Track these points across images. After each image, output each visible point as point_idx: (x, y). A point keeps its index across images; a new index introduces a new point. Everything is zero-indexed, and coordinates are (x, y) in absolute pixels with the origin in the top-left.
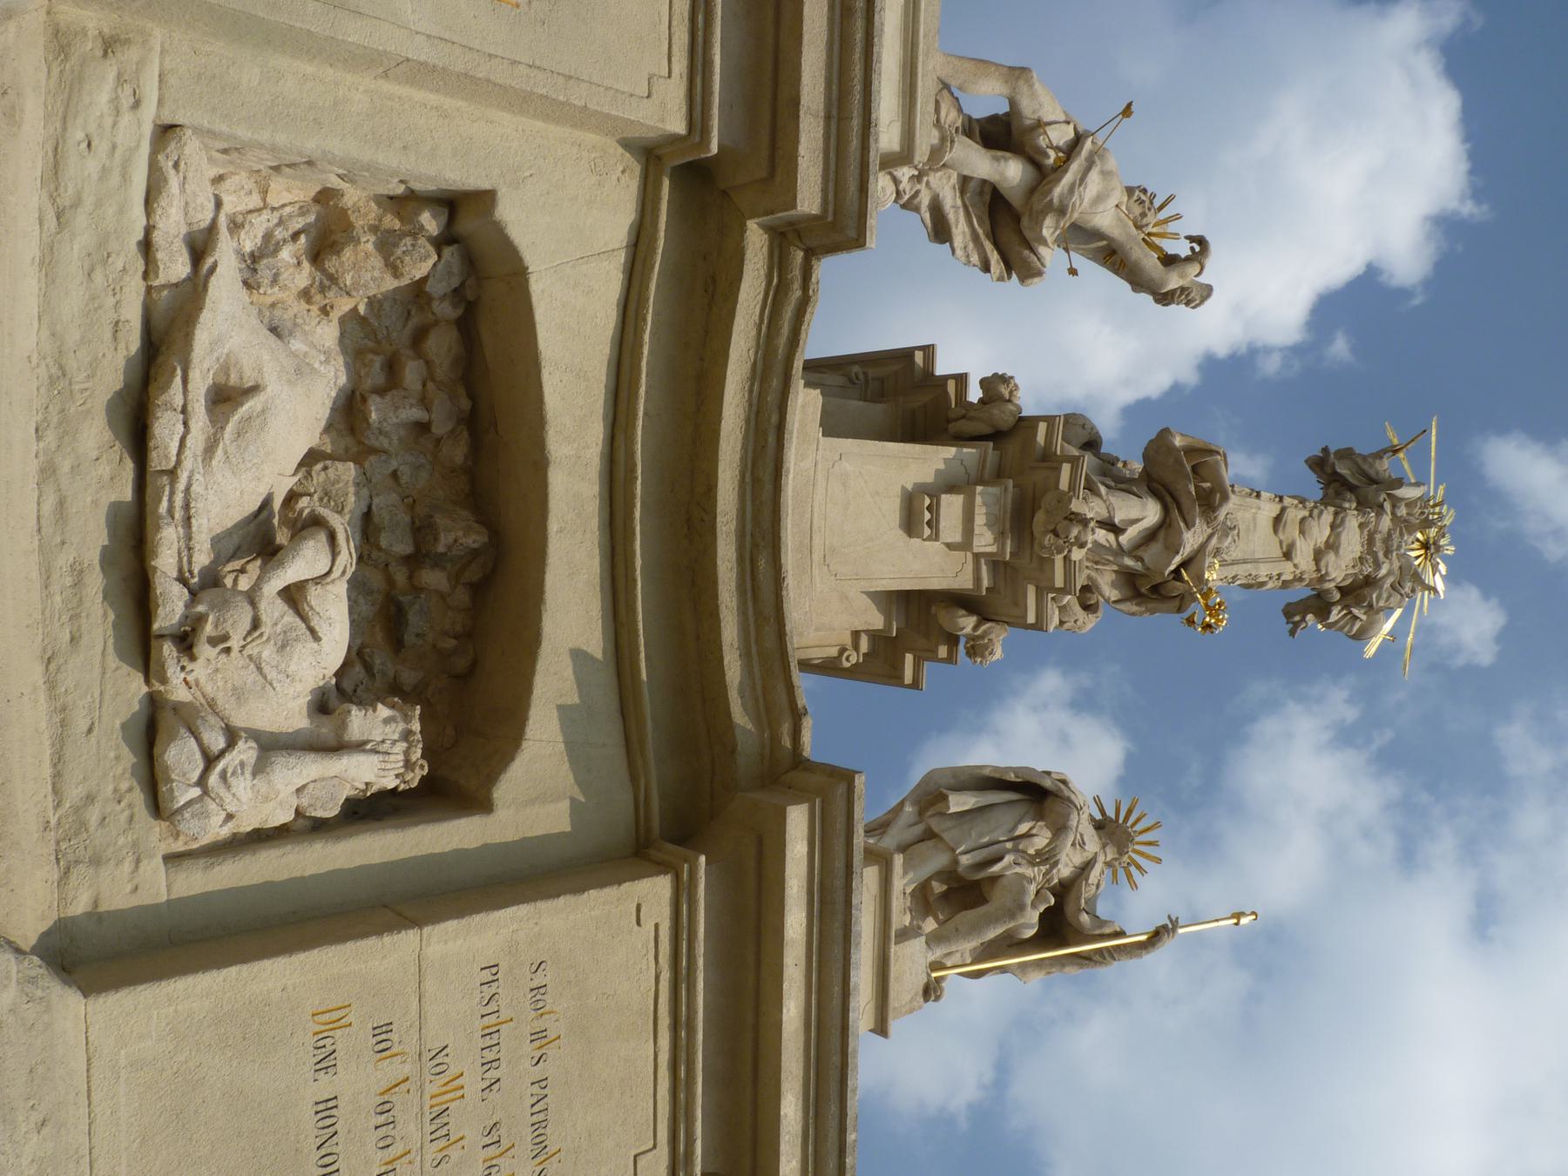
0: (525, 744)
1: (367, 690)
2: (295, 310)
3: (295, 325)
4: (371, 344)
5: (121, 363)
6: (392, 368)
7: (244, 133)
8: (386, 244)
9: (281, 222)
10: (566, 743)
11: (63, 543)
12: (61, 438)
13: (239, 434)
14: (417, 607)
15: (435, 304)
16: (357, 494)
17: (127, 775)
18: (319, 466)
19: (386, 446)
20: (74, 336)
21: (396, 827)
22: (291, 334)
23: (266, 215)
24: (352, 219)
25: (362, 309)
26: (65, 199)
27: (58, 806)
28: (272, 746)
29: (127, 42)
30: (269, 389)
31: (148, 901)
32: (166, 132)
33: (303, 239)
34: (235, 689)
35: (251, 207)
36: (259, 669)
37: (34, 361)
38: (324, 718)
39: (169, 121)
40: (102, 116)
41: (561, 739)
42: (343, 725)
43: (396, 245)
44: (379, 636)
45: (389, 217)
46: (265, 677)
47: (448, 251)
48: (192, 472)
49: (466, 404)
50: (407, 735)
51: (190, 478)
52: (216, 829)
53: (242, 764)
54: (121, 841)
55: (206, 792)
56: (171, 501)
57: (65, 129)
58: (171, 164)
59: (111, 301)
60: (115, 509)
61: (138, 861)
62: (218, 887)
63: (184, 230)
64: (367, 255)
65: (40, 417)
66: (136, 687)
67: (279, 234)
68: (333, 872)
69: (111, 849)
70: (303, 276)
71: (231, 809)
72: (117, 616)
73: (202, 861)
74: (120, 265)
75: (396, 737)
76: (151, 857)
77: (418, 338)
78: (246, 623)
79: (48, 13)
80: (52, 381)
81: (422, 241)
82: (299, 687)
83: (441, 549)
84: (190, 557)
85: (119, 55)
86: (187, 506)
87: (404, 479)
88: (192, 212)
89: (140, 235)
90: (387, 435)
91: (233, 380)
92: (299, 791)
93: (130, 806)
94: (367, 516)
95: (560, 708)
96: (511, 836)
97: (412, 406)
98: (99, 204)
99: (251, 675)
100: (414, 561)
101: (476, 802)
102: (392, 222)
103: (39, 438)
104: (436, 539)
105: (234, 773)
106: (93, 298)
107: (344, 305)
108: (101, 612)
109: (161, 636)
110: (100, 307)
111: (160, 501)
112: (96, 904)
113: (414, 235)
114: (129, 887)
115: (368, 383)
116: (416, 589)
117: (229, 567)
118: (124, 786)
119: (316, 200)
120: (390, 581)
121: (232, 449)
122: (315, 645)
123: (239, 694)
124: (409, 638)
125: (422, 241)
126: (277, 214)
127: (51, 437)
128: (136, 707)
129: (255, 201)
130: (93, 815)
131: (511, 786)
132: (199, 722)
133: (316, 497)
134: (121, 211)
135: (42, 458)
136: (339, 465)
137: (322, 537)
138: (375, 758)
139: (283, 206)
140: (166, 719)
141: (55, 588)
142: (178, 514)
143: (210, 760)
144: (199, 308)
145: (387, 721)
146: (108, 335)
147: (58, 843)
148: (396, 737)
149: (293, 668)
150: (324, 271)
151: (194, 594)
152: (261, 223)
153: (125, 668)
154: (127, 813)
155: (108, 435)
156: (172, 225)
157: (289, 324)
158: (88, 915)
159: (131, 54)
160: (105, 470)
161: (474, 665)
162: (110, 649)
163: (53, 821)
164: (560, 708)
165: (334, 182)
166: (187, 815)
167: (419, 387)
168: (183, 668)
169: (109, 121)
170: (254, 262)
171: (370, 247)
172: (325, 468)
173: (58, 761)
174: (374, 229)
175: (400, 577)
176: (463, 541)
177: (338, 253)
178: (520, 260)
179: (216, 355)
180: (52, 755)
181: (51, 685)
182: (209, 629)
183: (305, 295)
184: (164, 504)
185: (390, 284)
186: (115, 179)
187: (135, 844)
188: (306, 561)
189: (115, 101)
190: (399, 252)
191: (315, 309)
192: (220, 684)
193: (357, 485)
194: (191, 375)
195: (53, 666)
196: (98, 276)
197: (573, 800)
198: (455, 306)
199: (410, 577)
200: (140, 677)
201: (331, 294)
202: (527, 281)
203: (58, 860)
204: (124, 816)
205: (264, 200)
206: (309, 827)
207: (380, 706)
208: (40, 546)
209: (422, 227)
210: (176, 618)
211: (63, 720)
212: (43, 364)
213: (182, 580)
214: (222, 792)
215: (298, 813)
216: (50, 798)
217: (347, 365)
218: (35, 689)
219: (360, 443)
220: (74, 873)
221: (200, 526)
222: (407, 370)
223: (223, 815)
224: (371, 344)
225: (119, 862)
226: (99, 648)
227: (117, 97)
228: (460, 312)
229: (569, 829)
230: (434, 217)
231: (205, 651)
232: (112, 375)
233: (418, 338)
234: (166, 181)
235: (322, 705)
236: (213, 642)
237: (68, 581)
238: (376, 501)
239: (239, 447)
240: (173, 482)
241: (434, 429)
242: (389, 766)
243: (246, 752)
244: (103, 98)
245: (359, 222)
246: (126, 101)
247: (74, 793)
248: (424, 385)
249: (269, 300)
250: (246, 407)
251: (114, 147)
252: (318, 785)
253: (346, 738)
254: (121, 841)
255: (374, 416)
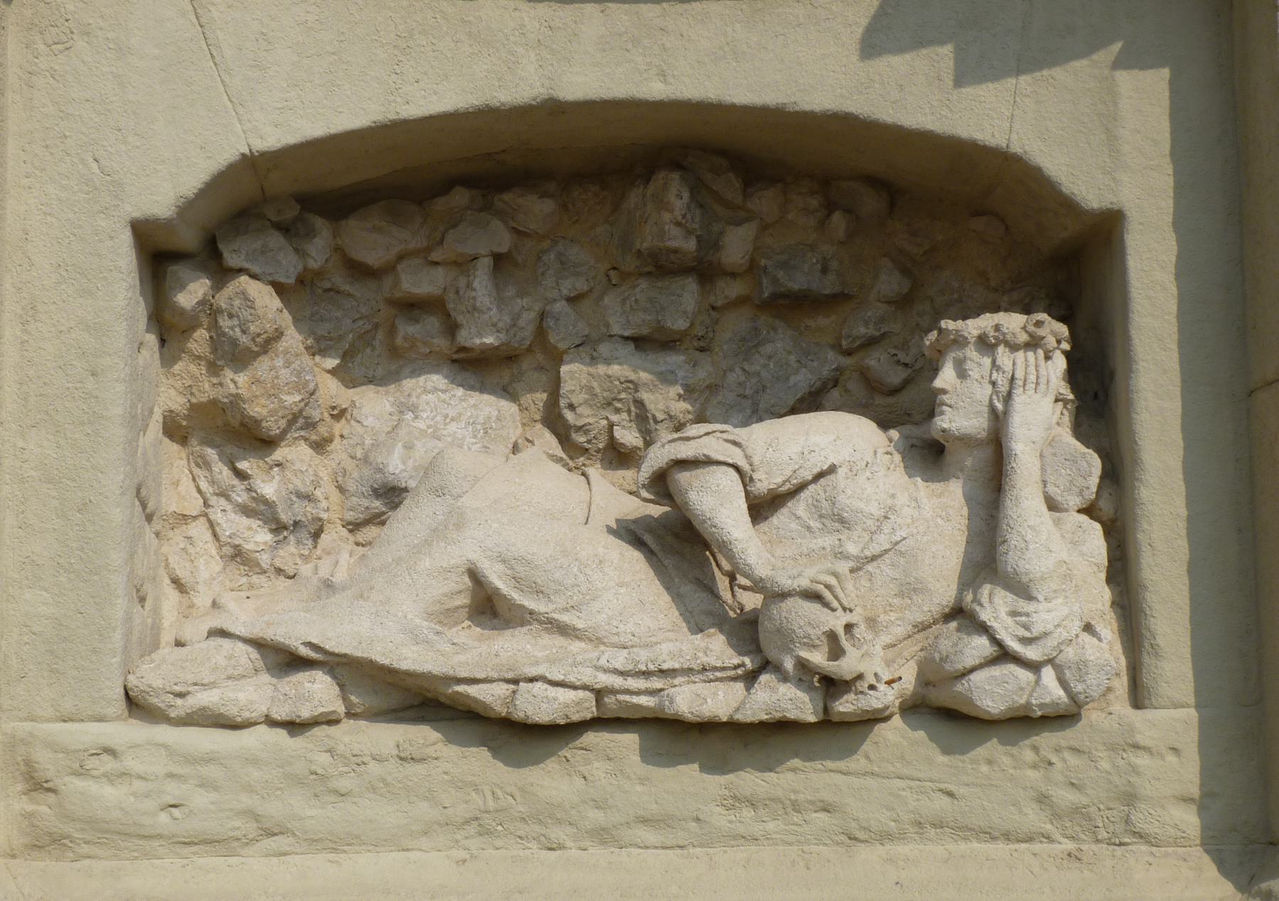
0: (1016, 148)
1: (904, 346)
2: (344, 456)
3: (366, 460)
4: (380, 335)
5: (453, 751)
6: (412, 307)
7: (118, 582)
8: (232, 354)
9: (224, 494)
10: (1019, 72)
11: (698, 820)
12: (559, 822)
13: (539, 592)
14: (780, 274)
15: (313, 264)
16: (608, 362)
17: (1015, 750)
18: (569, 416)
19: (532, 315)
20: (423, 810)
21: (1129, 370)
22: (380, 470)
23: (217, 516)
24: (203, 398)
25: (332, 363)
26: (250, 828)
27: (1049, 839)
28: (987, 558)
29: (28, 763)
30: (473, 556)
31: (1194, 734)
32: (135, 705)
33: (243, 465)
34: (901, 594)
35: (208, 536)
36: (874, 558)
37: (463, 854)
38: (948, 458)
39: (122, 704)
40: (134, 794)
41: (1011, 81)
42: (966, 441)
43: (234, 343)
44: (822, 321)
45: (191, 345)
46: (886, 551)
47: (232, 260)
48: (597, 668)
49: (460, 197)
50: (986, 344)
51: (605, 671)
52: (1104, 652)
53: (1014, 614)
54: (1105, 765)
55: (1050, 661)
56: (638, 693)
57: (160, 836)
58: (179, 702)
59: (373, 767)
60: (649, 755)
61: (1136, 747)
62: (1187, 639)
63: (265, 678)
64: (256, 381)
65: (533, 845)
66: (895, 731)
67: (241, 497)
68: (1185, 473)
69: (1115, 779)
70: (295, 453)
71: (1076, 627)
72: (796, 755)
73: (1146, 659)
74: (325, 758)
75: (987, 361)
76: (1132, 730)
77: (360, 271)
78: (813, 608)
79: (14, 857)
80: (485, 832)
81: (222, 300)
82: (902, 499)
83: (691, 245)
84: (716, 669)
85: (49, 775)
86: (646, 674)
87: (582, 285)
88: (240, 671)
89: (281, 734)
90: (516, 318)
91: (464, 600)
92: (1052, 505)
93: (1058, 750)
94: (639, 342)
95: (959, 82)
96: (1163, 180)
97: (469, 286)
98: (249, 789)
99: (883, 571)
100: (705, 271)
101: (1100, 236)
102: (200, 340)
103: (561, 847)
104: (675, 251)
105: (1026, 627)
106: (374, 789)
107: (331, 389)
108: (790, 775)
109: (826, 710)
110: (383, 780)
111: (640, 706)
112: (1188, 800)
113: (215, 312)
114: (1171, 758)
115: (441, 343)
116: (753, 268)
117: (726, 595)
118: (1029, 755)
119: (183, 441)
120: (741, 301)
121: (560, 601)
122: (842, 472)
123: (910, 589)
124: (828, 285)
125: (222, 300)
126: (213, 500)
127: (558, 833)
128: (921, 734)
129: (199, 530)
130: (1064, 797)
131: (1084, 179)
132: (948, 667)
133: (614, 418)
134: (254, 761)
135: (588, 844)
136: (566, 387)
137: (683, 477)
138: (1019, 399)
139: (199, 491)
140: (939, 697)
141: (757, 829)
142: (656, 683)
143: (1004, 655)
144: (371, 663)
145: (962, 374)
146: (419, 768)
147: (1098, 841)
148: (987, 361)
149: (874, 509)
150: (284, 432)
151: (766, 665)
152: (232, 523)
153: (867, 746)
154: (1067, 755)
155: (551, 764)
156: (257, 693)
157: (367, 472)
158: (1202, 809)
159: (47, 763)
160: (598, 769)
161: (875, 182)
162: (841, 765)
163: (1069, 846)
164: (959, 82)
165: (155, 427)
166: (1080, 688)
167: (440, 272)
168: (872, 687)
169: (138, 785)
170: (285, 528)
171: (242, 378)
172: (571, 407)
173: (989, 835)
174: (214, 369)
175: (734, 289)
176: (678, 214)
177: (257, 422)
178: (231, 167)
179: (432, 636)
180: (979, 840)
181: (885, 837)
182: (818, 658)
183: (320, 446)
184: (644, 700)
185: (293, 339)
186: (211, 771)
187: (1112, 748)
188: (718, 503)
189: (110, 778)
190: (244, 340)
191: (338, 427)
192: (893, 616)
193: (593, 360)
194: (463, 674)
195: (861, 835)
196: (344, 784)
197: (1118, 64)
198: (311, 233)
199: (733, 275)
200: (880, 728)
201: (315, 415)
202: (263, 154)
203: (1121, 844)
204: (1072, 760)
205: (195, 518)
206: (1114, 512)
207: (938, 383)
208: (701, 846)
209: (202, 303)
210: (802, 696)
211: (934, 825)
212: (466, 842)
213: (750, 678)
214: (1051, 642)
215: (1089, 511)
216: (1036, 847)
217: (415, 373)
218: (891, 860)
219: (529, 350)
220: (1141, 826)
221: (672, 655)
222: (415, 290)
223: (1086, 637)
224: (380, 335)
225: (1135, 770)
226: (839, 778)
227: (105, 775)
228: (319, 222)
229: (1165, 73)
230: (182, 287)
231: (846, 667)
232: (476, 763)
233: (360, 271)
234: (204, 709)
235: (930, 455)
236: (836, 652)
237: (748, 813)
238: (616, 330)
239: (556, 592)
240: (613, 691)
241: (503, 249)
242: (1032, 378)
243: (996, 607)
244: (110, 793)
245: (207, 390)
246: (108, 764)
247: (1034, 818)
248: (437, 263)
249: (335, 496)
250: (499, 584)
251: (171, 775)
252: (1051, 479)
253: (984, 434)
254: (1105, 765)
255: (489, 340)
